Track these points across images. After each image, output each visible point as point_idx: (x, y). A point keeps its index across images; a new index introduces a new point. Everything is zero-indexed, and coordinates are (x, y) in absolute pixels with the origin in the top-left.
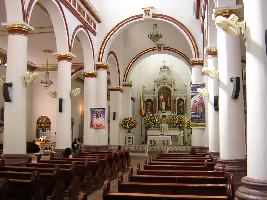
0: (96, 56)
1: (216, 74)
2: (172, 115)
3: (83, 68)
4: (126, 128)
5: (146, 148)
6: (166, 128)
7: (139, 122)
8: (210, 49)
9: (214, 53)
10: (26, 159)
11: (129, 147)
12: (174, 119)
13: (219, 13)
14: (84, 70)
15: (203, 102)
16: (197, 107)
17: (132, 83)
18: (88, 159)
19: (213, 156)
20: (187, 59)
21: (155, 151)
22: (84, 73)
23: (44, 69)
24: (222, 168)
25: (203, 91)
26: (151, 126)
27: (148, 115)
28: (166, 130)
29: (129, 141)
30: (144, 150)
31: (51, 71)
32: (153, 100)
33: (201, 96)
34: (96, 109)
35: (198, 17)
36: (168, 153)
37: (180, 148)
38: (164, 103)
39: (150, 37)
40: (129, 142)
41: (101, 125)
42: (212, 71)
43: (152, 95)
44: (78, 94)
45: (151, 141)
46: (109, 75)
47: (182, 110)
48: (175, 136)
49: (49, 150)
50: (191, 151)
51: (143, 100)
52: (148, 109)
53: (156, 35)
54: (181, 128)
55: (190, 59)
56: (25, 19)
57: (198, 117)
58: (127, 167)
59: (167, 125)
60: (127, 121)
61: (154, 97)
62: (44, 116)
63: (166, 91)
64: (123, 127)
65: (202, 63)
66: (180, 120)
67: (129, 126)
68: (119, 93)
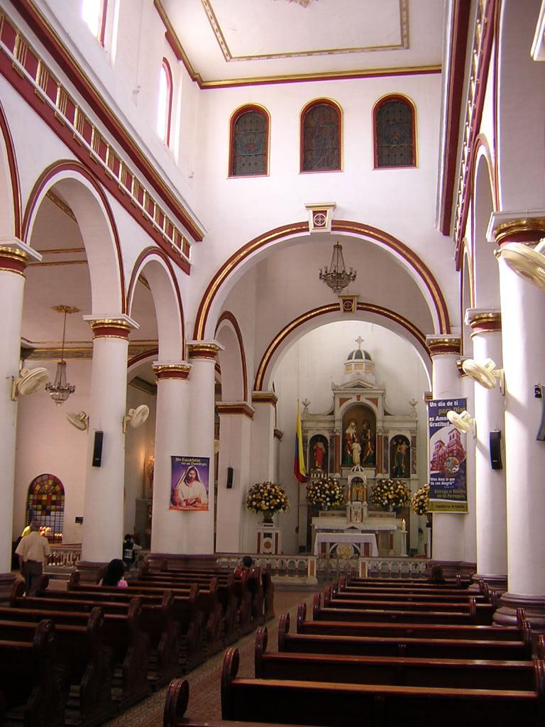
0: (187, 323)
1: (498, 379)
2: (377, 477)
3: (155, 351)
4: (258, 509)
5: (312, 562)
6: (362, 511)
7: (293, 495)
8: (479, 312)
9: (493, 324)
10: (12, 586)
11: (267, 559)
12: (382, 488)
13: (505, 226)
14: (157, 360)
15: (461, 446)
16: (445, 459)
17: (276, 394)
18: (172, 591)
19: (490, 588)
20: (421, 337)
21: (333, 570)
22: (158, 366)
23: (51, 353)
24: (515, 619)
25: (463, 417)
26: (323, 504)
27: (317, 476)
28: (362, 517)
29: (268, 545)
30: (307, 569)
31: (69, 360)
32: (328, 439)
33: (454, 432)
34: (186, 460)
35: (446, 231)
36: (368, 576)
37: (399, 564)
38: (357, 447)
39: (324, 277)
40: (266, 547)
41: (198, 500)
42: (488, 370)
43: (327, 425)
44: (141, 420)
45: (323, 545)
46: (220, 372)
47: (403, 465)
48: (385, 532)
49: (60, 562)
50: (430, 573)
51: (303, 437)
52: (315, 461)
53: (340, 274)
54: (401, 512)
55: (428, 337)
56: (20, 231)
57: (447, 484)
58: (264, 613)
59: (365, 503)
60: (262, 490)
61: (332, 431)
62: (49, 475)
63: (362, 416)
64: (251, 506)
65: (456, 347)
66: (400, 492)
67: (268, 504)
68: (243, 418)
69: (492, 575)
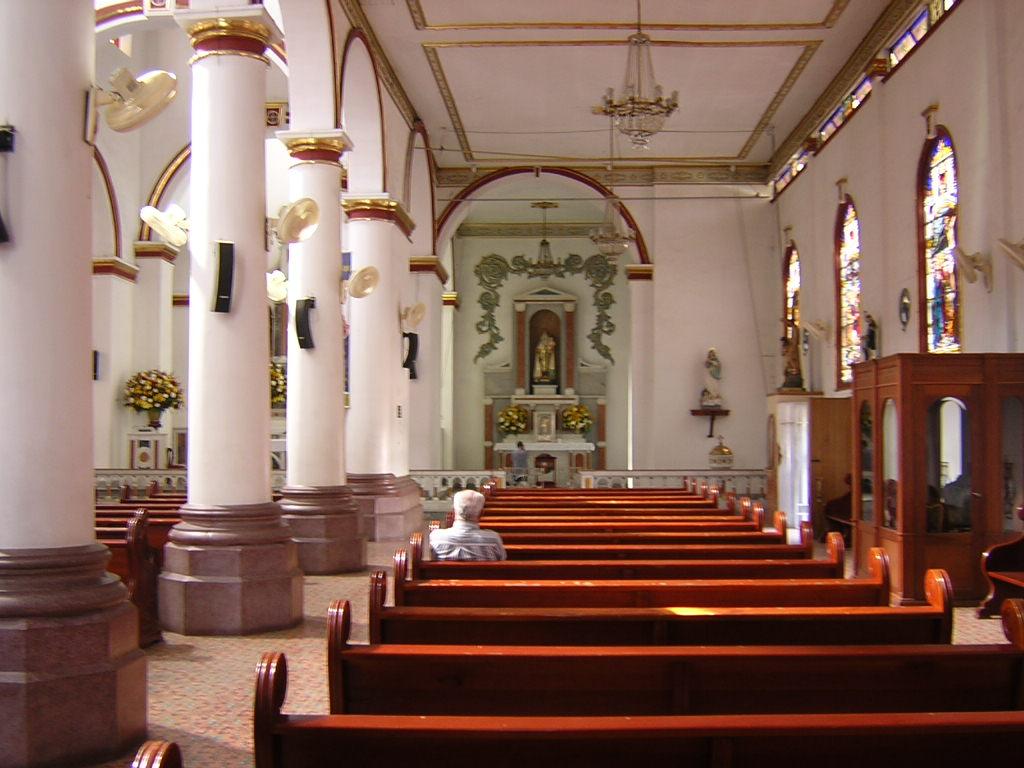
8: (296, 136)
29: (144, 457)
67: (150, 400)
69: (300, 487)
